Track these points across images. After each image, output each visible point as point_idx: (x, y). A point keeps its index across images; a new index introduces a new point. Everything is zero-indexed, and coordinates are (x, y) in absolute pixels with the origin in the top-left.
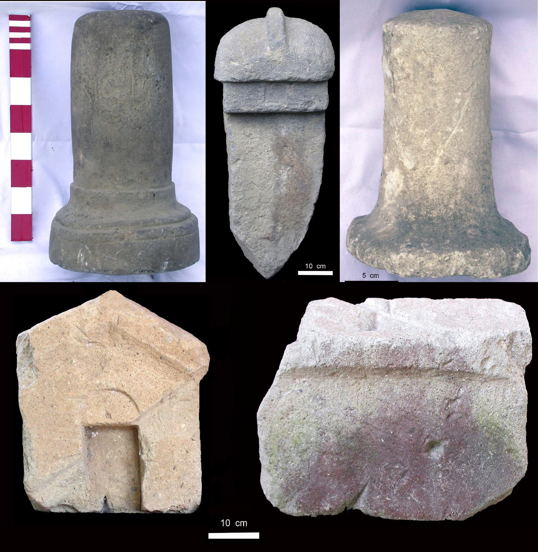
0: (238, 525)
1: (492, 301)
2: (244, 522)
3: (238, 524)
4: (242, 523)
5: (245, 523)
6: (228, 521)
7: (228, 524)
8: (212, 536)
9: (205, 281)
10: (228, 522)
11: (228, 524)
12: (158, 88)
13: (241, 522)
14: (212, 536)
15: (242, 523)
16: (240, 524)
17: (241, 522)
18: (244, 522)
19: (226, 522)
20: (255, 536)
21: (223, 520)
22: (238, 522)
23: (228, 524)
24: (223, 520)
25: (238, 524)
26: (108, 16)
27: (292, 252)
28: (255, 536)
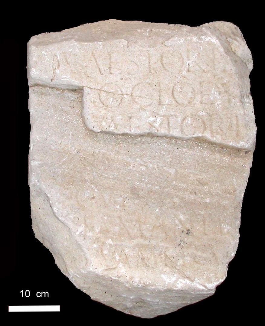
0: (39, 296)
1: (236, 243)
2: (45, 293)
3: (39, 295)
4: (44, 294)
5: (47, 294)
6: (28, 292)
7: (28, 295)
8: (12, 309)
9: (59, 306)
10: (28, 292)
11: (28, 295)
12: (151, 264)
13: (42, 293)
14: (12, 309)
15: (44, 294)
16: (41, 294)
17: (42, 293)
18: (45, 293)
19: (26, 293)
20: (56, 308)
21: (22, 291)
22: (39, 293)
23: (27, 295)
24: (22, 291)
25: (39, 295)
26: (173, 31)
27: (210, 23)
28: (56, 308)
